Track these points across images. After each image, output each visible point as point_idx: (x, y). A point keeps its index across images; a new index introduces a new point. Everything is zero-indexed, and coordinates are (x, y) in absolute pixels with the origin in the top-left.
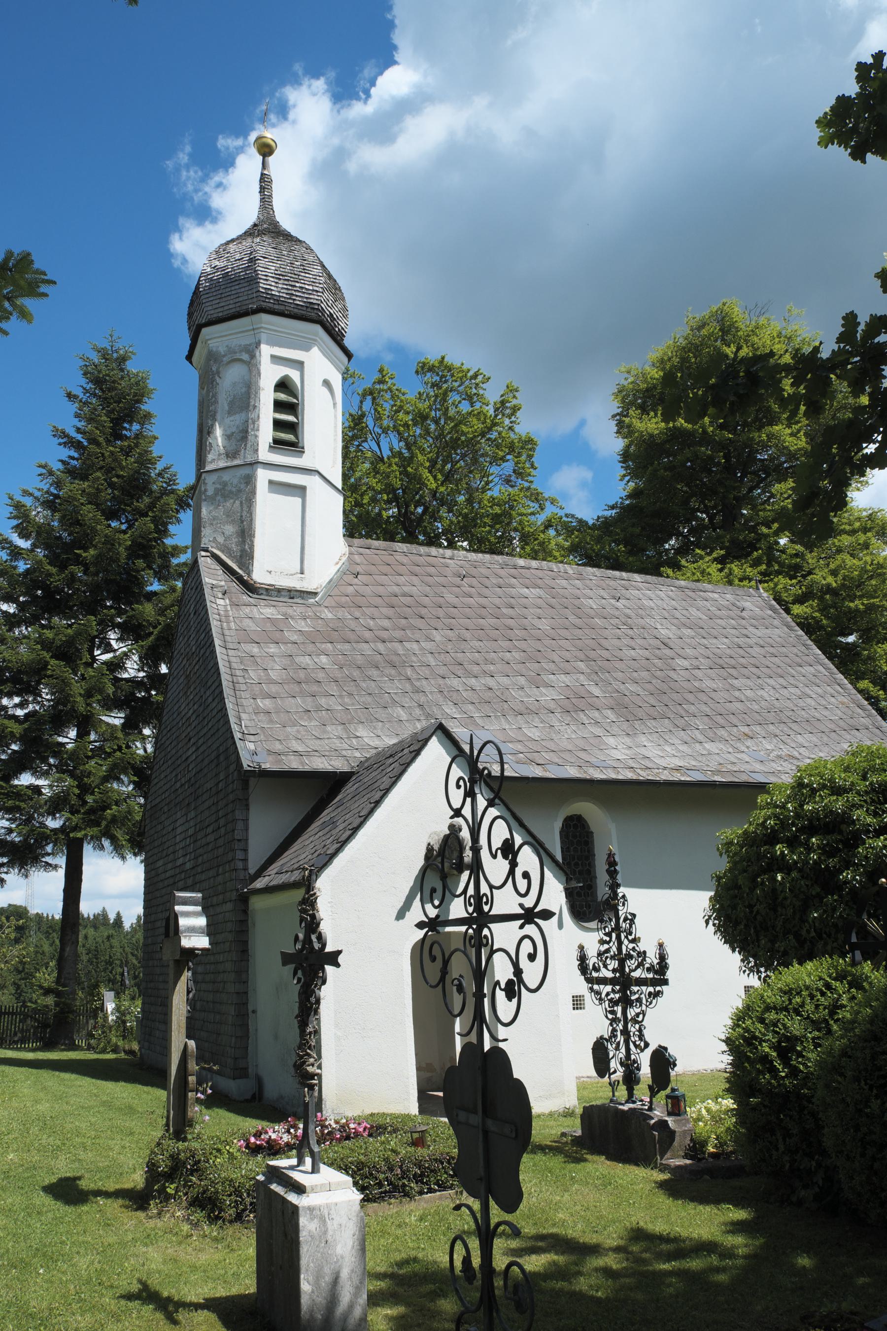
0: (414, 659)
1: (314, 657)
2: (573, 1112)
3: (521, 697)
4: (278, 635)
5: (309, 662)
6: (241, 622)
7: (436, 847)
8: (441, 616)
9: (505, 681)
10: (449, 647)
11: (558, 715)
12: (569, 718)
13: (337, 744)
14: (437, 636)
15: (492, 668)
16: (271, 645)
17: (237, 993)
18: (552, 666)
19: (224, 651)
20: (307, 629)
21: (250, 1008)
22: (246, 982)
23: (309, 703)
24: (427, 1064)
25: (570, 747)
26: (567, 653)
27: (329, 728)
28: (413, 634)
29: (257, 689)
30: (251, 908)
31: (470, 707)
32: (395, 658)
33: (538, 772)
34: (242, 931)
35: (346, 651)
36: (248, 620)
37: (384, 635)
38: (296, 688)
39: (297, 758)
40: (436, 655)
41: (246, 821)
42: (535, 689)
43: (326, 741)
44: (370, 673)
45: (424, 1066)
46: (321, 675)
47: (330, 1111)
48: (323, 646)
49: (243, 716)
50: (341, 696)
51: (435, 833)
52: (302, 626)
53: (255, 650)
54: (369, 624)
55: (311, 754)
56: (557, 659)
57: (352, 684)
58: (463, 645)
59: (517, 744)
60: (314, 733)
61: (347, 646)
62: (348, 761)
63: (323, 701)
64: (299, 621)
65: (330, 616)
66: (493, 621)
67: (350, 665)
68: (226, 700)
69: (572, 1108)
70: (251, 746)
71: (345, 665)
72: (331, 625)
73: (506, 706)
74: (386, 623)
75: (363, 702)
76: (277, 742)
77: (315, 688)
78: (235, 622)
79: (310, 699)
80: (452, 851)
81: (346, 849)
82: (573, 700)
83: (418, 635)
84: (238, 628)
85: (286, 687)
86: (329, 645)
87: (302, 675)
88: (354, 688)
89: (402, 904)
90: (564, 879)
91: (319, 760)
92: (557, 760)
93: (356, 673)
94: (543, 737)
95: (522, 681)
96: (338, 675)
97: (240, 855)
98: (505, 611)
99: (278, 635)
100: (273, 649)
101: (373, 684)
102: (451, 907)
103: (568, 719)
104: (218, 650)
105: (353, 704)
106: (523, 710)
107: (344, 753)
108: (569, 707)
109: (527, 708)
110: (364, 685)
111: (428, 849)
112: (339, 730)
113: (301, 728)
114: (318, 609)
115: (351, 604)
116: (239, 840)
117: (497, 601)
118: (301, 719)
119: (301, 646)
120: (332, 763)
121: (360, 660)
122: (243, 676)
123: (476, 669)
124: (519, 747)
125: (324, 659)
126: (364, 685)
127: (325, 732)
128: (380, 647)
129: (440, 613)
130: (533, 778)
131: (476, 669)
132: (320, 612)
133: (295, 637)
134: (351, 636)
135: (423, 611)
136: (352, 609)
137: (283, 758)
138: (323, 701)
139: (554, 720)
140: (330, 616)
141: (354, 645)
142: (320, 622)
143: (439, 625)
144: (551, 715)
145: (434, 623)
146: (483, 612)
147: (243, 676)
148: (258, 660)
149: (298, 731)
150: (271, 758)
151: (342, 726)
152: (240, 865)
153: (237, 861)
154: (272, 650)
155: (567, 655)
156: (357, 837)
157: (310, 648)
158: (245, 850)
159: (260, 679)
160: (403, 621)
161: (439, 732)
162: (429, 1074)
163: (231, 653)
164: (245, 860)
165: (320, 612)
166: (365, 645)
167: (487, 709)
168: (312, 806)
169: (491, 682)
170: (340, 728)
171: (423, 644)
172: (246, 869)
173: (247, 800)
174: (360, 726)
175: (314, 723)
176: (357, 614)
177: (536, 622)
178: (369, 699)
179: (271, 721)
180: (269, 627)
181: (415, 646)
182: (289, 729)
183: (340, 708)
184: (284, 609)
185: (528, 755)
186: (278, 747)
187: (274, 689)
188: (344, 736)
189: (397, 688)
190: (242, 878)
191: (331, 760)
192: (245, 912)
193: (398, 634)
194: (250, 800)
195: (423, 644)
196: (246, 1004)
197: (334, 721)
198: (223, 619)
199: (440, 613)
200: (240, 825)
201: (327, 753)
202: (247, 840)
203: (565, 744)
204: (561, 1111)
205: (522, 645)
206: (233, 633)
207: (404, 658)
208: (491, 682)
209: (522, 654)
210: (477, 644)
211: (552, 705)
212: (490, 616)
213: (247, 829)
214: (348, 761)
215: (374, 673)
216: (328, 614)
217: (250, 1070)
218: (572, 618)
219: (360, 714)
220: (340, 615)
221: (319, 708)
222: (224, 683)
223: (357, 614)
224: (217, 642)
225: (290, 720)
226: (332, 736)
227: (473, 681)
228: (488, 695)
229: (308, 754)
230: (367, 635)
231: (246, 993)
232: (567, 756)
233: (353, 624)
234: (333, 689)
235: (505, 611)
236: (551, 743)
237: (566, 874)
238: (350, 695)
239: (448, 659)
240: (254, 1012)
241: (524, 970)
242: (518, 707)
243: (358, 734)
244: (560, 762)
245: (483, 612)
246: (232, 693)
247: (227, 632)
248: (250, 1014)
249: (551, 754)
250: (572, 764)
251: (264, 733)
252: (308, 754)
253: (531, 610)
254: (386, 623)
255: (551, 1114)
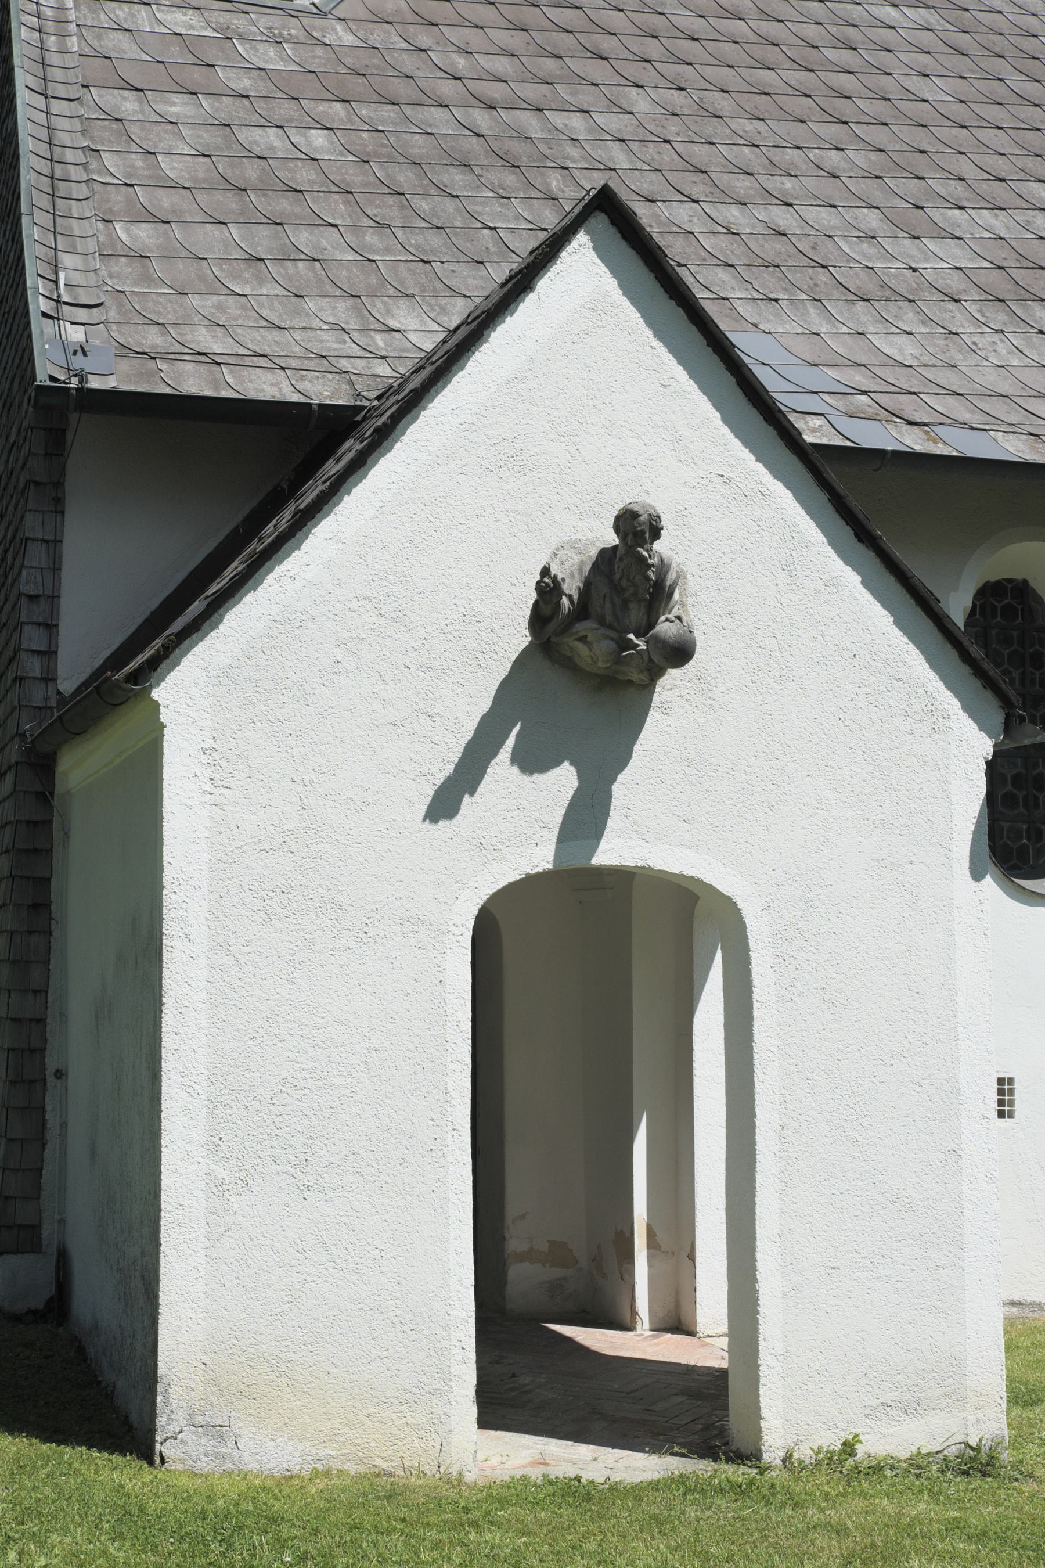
0: (573, 152)
1: (292, 133)
2: (991, 1460)
3: (870, 259)
4: (198, 75)
5: (277, 143)
6: (99, 38)
7: (572, 587)
8: (654, 56)
9: (824, 217)
10: (673, 129)
11: (973, 308)
12: (1002, 317)
13: (330, 342)
14: (640, 102)
15: (788, 184)
16: (175, 98)
17: (14, 1020)
18: (957, 190)
19: (40, 102)
20: (281, 66)
21: (51, 1065)
22: (41, 992)
23: (263, 242)
24: (552, 1243)
25: (1004, 388)
26: (1001, 160)
27: (311, 304)
28: (573, 94)
29: (118, 198)
30: (59, 789)
31: (722, 274)
32: (518, 149)
33: (914, 441)
34: (36, 851)
35: (383, 122)
36: (120, 35)
37: (495, 91)
38: (230, 202)
39: (203, 368)
40: (635, 146)
41: (54, 544)
42: (908, 242)
43: (298, 335)
44: (445, 178)
45: (544, 1247)
46: (304, 176)
47: (180, 1417)
48: (322, 107)
49: (67, 260)
50: (355, 228)
51: (573, 545)
52: (269, 57)
53: (128, 105)
54: (453, 64)
55: (247, 361)
56: (969, 171)
57: (391, 200)
58: (711, 128)
59: (851, 371)
60: (265, 313)
61: (388, 112)
62: (352, 383)
63: (303, 238)
64: (262, 48)
65: (348, 39)
66: (797, 77)
67: (389, 156)
68: (25, 220)
69: (987, 1443)
70: (76, 335)
71: (377, 155)
72: (348, 61)
73: (822, 276)
74: (501, 65)
75: (417, 247)
76: (155, 329)
77: (284, 205)
78: (81, 36)
79: (265, 232)
80: (625, 603)
81: (270, 579)
82: (1014, 273)
83: (586, 97)
84: (87, 50)
85: (202, 197)
86: (338, 106)
87: (251, 171)
88: (395, 212)
89: (450, 768)
90: (999, 718)
91: (269, 376)
92: (965, 416)
93: (405, 177)
94: (927, 359)
95: (871, 220)
96: (355, 177)
97: (33, 638)
98: (830, 54)
99: (198, 75)
100: (178, 107)
101: (450, 205)
102: (615, 788)
103: (998, 317)
104: (23, 98)
105: (388, 250)
106: (870, 287)
107: (344, 364)
108: (1003, 287)
109: (884, 286)
110: (423, 205)
111: (540, 587)
112: (341, 311)
113: (231, 300)
114: (319, 22)
115: (410, 17)
116: (33, 598)
117: (811, 32)
118: (237, 277)
119: (260, 105)
120: (306, 386)
121: (419, 147)
122: (85, 165)
123: (742, 185)
124: (858, 379)
125: (318, 139)
126: (423, 205)
127: (297, 312)
128: (481, 119)
129: (653, 49)
130: (896, 453)
131: (742, 185)
132: (323, 30)
133: (244, 83)
134: (402, 89)
135: (607, 44)
136: (411, 28)
137: (162, 365)
138: (303, 238)
139: (956, 318)
140: (348, 39)
141: (408, 110)
142: (319, 51)
143: (647, 75)
144: (952, 306)
145: (633, 71)
146: (772, 55)
147: (85, 165)
148: (134, 130)
149: (220, 307)
150: (124, 366)
151: (350, 302)
152: (34, 667)
153: (23, 656)
154: (174, 109)
155: (1001, 166)
156: (307, 545)
157: (285, 110)
158: (50, 627)
159: (129, 175)
160: (550, 64)
161: (600, 221)
162: (554, 1273)
163: (56, 107)
164: (49, 654)
165: (323, 30)
166: (438, 114)
167: (769, 282)
168: (245, 511)
169: (782, 218)
170: (342, 305)
171: (599, 119)
172: (49, 678)
173: (59, 485)
174: (403, 303)
175: (269, 289)
176: (424, 38)
177: (916, 84)
178: (435, 240)
179: (146, 278)
180: (175, 53)
181: (577, 122)
182: (195, 300)
183: (351, 256)
184: (223, 18)
185: (882, 399)
186: (152, 339)
187: (166, 201)
188: (351, 326)
189: (519, 216)
190: (38, 701)
191: (302, 379)
192: (45, 796)
193: (533, 92)
194: (68, 487)
195: (599, 119)
196: (39, 1051)
197: (331, 289)
198: (50, 26)
199: (653, 49)
200: (36, 555)
201: (294, 363)
202: (54, 598)
203: (991, 379)
204: (952, 1452)
205: (878, 135)
206: (70, 61)
207: (543, 147)
208: (782, 218)
209: (874, 156)
210: (751, 127)
211: (955, 283)
212: (788, 64)
213: (56, 568)
214: (352, 383)
215: (456, 179)
216: (342, 35)
217: (45, 1233)
218: (1014, 80)
219: (405, 274)
220: (376, 40)
221: (290, 256)
222: (26, 177)
223: (424, 38)
224: (22, 79)
225: (202, 278)
226: (316, 323)
227: (733, 214)
228: (773, 249)
229: (238, 361)
230: (448, 89)
231: (41, 1021)
232: (997, 407)
233: (409, 63)
234: (337, 210)
235: (830, 54)
236: (950, 373)
237: (1005, 702)
238: (383, 226)
239: (666, 156)
240: (59, 1074)
241: (526, 779)
242: (859, 281)
243: (393, 323)
244: (977, 420)
245: (772, 55)
246: (44, 202)
247: (53, 59)
248: (51, 1080)
249: (951, 400)
250: (1012, 430)
251: (120, 305)
252: (238, 361)
253: (902, 56)
254: (501, 65)
255: (918, 1464)
